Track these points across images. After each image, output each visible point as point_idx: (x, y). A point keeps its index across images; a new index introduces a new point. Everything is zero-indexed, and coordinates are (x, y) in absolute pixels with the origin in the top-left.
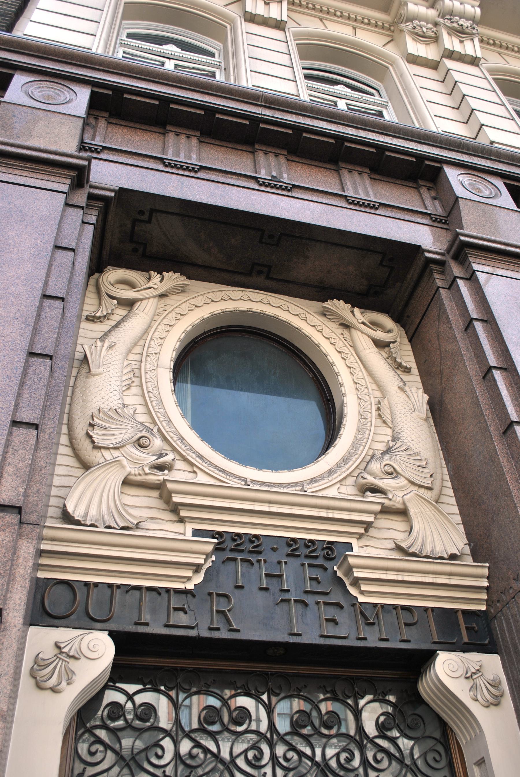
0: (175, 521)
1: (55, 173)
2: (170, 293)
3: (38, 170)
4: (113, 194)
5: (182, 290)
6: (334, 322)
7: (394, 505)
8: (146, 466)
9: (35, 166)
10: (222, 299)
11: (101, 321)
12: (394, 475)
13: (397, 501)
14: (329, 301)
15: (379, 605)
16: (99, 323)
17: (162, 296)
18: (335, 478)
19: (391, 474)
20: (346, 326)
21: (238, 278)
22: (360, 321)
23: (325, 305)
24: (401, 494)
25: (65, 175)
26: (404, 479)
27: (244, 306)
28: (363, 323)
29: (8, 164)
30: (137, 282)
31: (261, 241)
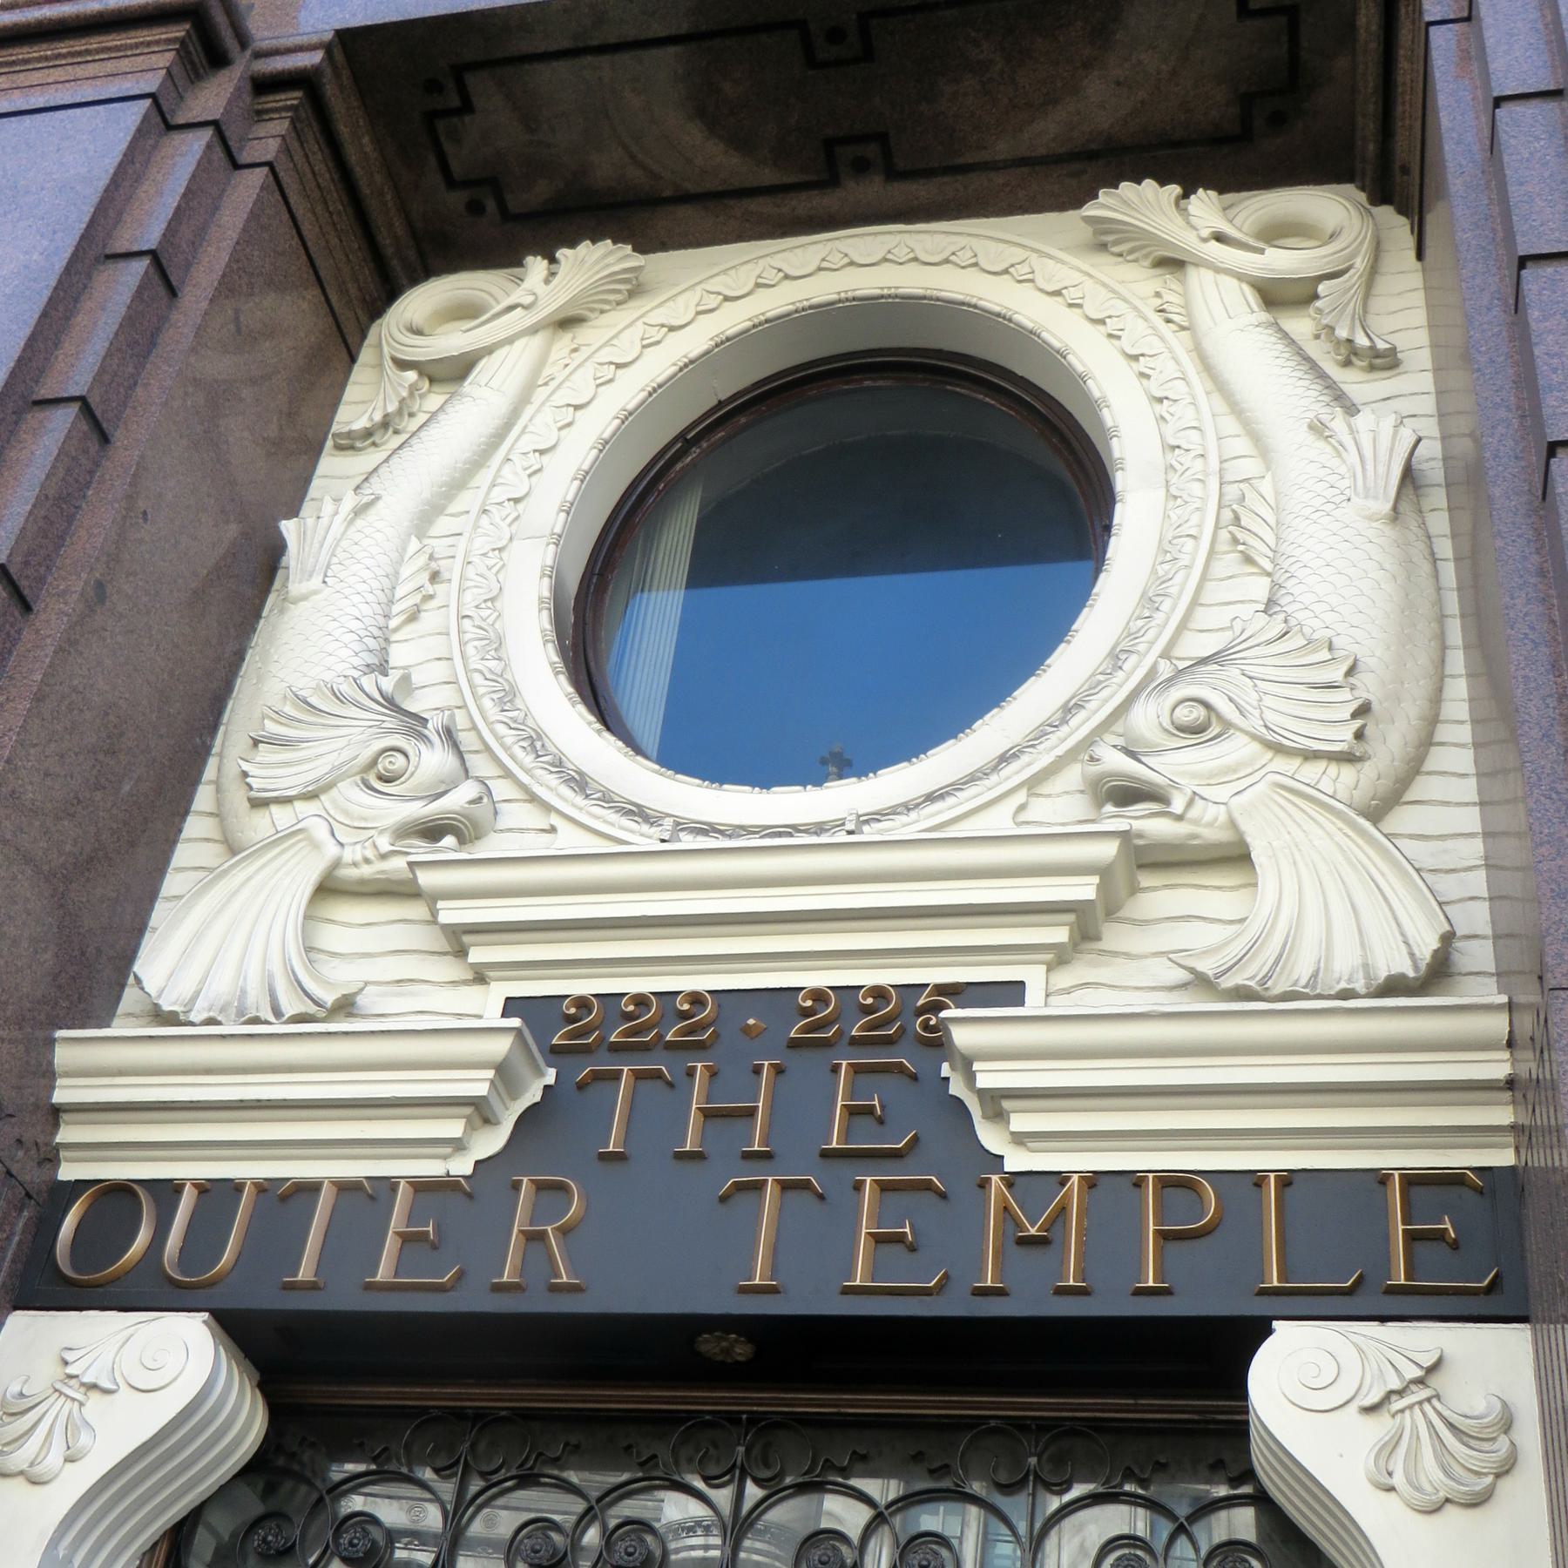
0: (465, 982)
1: (131, 47)
2: (592, 310)
3: (88, 52)
4: (316, 58)
5: (636, 289)
6: (1135, 261)
7: (1195, 836)
8: (382, 832)
9: (79, 45)
10: (758, 285)
11: (374, 444)
12: (1215, 729)
13: (1208, 818)
14: (1104, 195)
15: (1075, 1177)
16: (372, 449)
17: (567, 322)
18: (1008, 778)
19: (1196, 730)
20: (1173, 264)
21: (802, 204)
22: (1205, 233)
23: (1090, 210)
24: (1222, 793)
25: (157, 42)
26: (1246, 739)
27: (823, 289)
28: (1219, 238)
29: (13, 63)
30: (486, 296)
31: (812, 62)
